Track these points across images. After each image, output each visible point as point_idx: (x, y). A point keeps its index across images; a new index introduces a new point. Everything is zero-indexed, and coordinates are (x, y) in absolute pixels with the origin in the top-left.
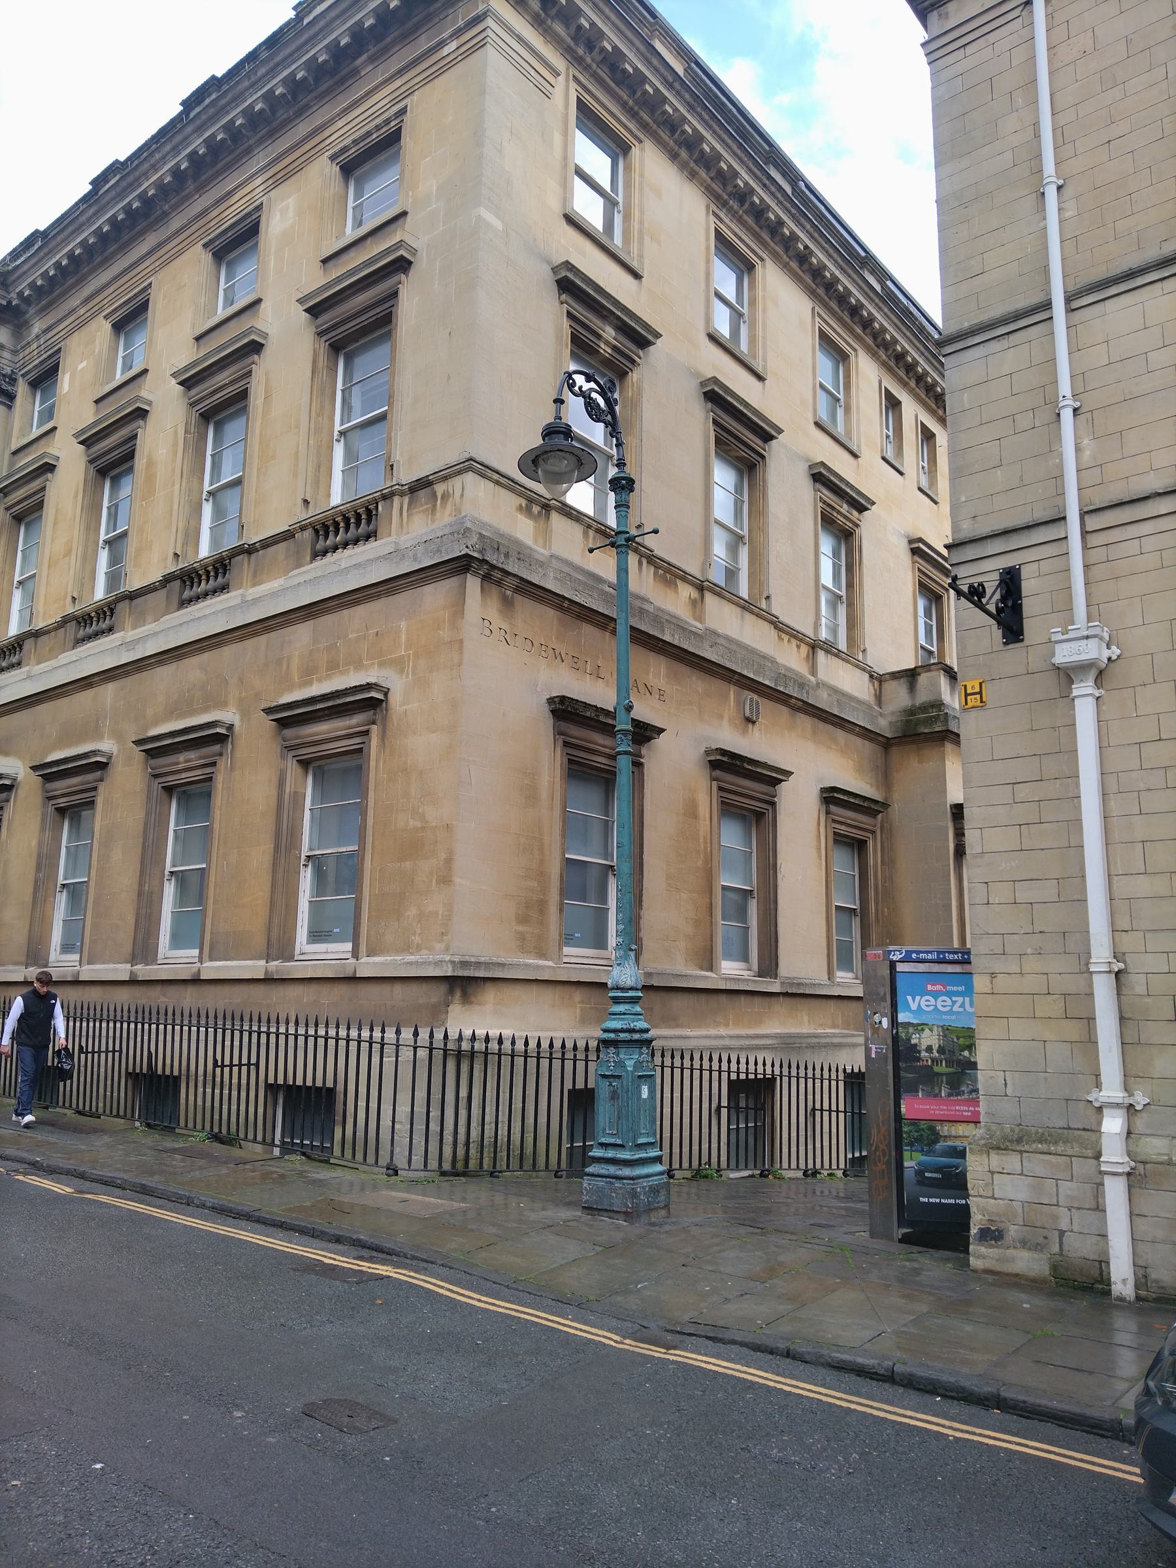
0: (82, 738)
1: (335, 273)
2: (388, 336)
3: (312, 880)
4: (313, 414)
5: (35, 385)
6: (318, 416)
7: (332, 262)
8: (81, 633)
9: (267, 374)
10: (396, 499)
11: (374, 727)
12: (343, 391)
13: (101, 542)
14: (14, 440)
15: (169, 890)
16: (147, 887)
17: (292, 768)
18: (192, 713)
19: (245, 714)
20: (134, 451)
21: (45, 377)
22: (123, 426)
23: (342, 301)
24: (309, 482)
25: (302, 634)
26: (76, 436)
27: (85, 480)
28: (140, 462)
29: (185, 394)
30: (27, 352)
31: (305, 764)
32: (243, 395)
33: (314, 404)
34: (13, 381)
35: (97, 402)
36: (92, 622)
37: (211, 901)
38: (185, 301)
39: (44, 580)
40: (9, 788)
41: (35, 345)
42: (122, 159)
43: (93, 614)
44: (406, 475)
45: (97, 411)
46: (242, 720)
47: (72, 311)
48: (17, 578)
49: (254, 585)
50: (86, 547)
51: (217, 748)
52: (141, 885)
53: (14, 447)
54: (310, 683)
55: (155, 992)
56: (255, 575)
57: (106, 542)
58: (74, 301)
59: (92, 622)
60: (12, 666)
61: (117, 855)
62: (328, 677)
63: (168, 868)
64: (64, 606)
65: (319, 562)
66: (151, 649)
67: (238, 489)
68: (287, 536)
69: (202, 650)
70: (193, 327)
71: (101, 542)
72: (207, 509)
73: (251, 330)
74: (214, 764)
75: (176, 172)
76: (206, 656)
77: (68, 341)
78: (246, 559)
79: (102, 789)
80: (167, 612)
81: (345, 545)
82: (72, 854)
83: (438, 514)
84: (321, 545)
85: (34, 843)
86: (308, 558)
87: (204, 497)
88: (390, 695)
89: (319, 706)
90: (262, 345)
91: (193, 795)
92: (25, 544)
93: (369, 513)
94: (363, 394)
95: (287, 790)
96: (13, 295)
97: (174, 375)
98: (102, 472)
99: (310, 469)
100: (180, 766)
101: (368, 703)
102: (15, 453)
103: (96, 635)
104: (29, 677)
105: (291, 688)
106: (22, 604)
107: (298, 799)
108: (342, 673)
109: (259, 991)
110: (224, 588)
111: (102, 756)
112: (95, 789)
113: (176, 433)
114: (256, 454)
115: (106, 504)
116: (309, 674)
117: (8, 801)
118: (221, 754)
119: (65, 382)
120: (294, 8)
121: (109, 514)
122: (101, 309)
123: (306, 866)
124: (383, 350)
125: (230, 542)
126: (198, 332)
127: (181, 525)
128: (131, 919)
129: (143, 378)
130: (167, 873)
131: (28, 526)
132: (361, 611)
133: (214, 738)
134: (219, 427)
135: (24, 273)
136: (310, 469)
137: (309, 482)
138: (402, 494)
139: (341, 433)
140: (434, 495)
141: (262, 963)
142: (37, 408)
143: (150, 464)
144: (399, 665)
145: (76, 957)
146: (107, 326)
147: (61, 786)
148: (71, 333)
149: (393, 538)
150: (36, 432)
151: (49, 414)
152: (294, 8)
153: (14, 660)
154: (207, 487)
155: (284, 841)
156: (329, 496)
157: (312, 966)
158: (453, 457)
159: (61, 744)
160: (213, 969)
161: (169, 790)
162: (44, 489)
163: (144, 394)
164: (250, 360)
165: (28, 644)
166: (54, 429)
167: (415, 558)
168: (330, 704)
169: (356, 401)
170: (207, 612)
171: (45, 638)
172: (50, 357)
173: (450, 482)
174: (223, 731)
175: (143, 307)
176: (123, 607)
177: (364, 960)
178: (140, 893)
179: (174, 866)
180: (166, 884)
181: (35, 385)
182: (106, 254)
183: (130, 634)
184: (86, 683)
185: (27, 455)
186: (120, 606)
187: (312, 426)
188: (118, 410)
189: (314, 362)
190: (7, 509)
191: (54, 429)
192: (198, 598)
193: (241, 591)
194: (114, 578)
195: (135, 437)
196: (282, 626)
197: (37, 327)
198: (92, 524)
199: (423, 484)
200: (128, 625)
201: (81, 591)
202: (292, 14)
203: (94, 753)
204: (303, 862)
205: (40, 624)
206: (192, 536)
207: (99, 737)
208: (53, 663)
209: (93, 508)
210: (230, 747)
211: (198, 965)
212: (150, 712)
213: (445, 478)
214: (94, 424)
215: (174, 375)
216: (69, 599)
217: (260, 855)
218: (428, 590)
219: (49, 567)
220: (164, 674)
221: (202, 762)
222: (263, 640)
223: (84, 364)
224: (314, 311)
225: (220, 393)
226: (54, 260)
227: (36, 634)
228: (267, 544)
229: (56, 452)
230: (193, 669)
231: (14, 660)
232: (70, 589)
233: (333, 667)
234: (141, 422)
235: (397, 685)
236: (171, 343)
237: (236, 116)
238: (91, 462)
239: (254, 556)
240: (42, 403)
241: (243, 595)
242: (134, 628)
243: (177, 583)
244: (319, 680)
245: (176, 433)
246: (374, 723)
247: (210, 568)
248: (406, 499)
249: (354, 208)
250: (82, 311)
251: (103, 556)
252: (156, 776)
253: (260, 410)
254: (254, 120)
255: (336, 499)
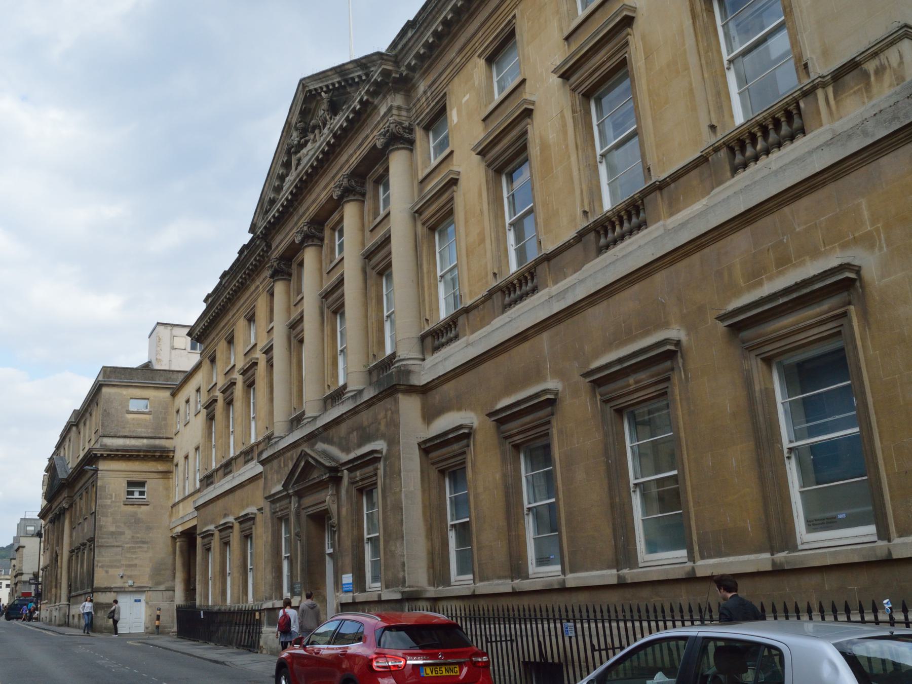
0: (526, 382)
1: (574, 48)
2: (626, 75)
3: (534, 521)
4: (702, 52)
5: (427, 129)
6: (706, 52)
7: (573, 38)
8: (507, 299)
9: (643, 38)
10: (820, 93)
11: (852, 307)
12: (598, 125)
13: (507, 225)
14: (420, 172)
15: (530, 523)
16: (617, 500)
17: (756, 366)
18: (632, 339)
19: (690, 328)
20: (526, 144)
21: (437, 117)
22: (518, 123)
23: (588, 59)
24: (712, 109)
25: (741, 241)
26: (474, 149)
27: (487, 181)
28: (534, 150)
29: (564, 84)
30: (418, 106)
31: (768, 361)
32: (623, 63)
33: (701, 44)
34: (411, 130)
35: (484, 120)
36: (513, 291)
37: (691, 504)
38: (470, 97)
39: (465, 267)
40: (467, 436)
41: (424, 99)
42: (411, 19)
43: (515, 282)
44: (821, 68)
45: (486, 127)
46: (688, 335)
47: (452, 62)
48: (439, 274)
49: (672, 214)
50: (497, 232)
51: (668, 364)
52: (612, 498)
53: (421, 177)
54: (760, 284)
55: (645, 593)
56: (670, 205)
57: (511, 224)
58: (451, 54)
59: (513, 291)
60: (450, 341)
61: (580, 475)
62: (780, 273)
63: (632, 481)
64: (487, 282)
65: (742, 175)
66: (580, 294)
67: (532, 215)
68: (702, 160)
69: (633, 283)
70: (561, 30)
71: (507, 225)
72: (603, 170)
73: (451, 172)
74: (668, 379)
75: (445, 22)
76: (637, 287)
77: (450, 86)
78: (659, 195)
79: (554, 422)
80: (587, 260)
81: (631, 233)
82: (456, 502)
83: (875, 90)
84: (603, 241)
85: (498, 476)
86: (729, 174)
87: (598, 160)
88: (863, 272)
89: (781, 301)
90: (532, 110)
91: (538, 449)
92: (440, 247)
93: (789, 115)
94: (737, 25)
95: (757, 388)
96: (403, 68)
97: (554, 72)
98: (499, 172)
99: (710, 98)
100: (632, 388)
101: (844, 284)
102: (421, 182)
103: (521, 298)
104: (468, 345)
105: (738, 293)
106: (446, 293)
107: (769, 394)
108: (795, 266)
109: (766, 585)
110: (534, 290)
111: (551, 393)
112: (549, 422)
113: (563, 117)
114: (648, 107)
115: (505, 195)
116: (755, 276)
117: (468, 446)
118: (672, 369)
119: (453, 116)
120: (205, 301)
121: (509, 202)
122: (475, 51)
123: (789, 458)
124: (627, 83)
125: (532, 255)
126: (566, 34)
127: (584, 187)
128: (608, 531)
129: (522, 87)
130: (632, 485)
131: (598, 102)
132: (805, 202)
133: (667, 356)
134: (598, 102)
135: (410, 49)
136: (710, 98)
137: (712, 109)
138: (824, 85)
139: (602, 156)
140: (866, 75)
141: (767, 556)
142: (432, 145)
143: (545, 147)
144: (868, 241)
145: (470, 576)
146: (482, 62)
147: (514, 426)
148: (451, 80)
149: (826, 127)
150: (434, 163)
151: (444, 144)
152: (205, 301)
153: (452, 335)
154: (599, 151)
155: (764, 437)
156: (732, 116)
157: (830, 553)
158: (879, 31)
159: (507, 392)
160: (574, 579)
161: (517, 447)
162: (452, 199)
163: (527, 96)
164: (624, 33)
165: (461, 320)
166: (452, 152)
167: (865, 133)
168: (794, 295)
169: (609, 132)
170: (630, 249)
171: (475, 312)
172: (437, 103)
173: (882, 56)
174: (672, 348)
175: (512, 34)
176: (543, 269)
177: (897, 541)
178: (612, 506)
179: (529, 503)
180: (633, 494)
181: (427, 129)
182: (470, 11)
183: (554, 289)
184: (522, 337)
185: (433, 179)
186: (539, 269)
187: (704, 62)
188: (508, 117)
189: (693, 10)
190: (423, 224)
191: (452, 152)
192: (615, 242)
193: (661, 223)
194: (521, 253)
195: (526, 132)
196: (716, 240)
197: (422, 87)
198: (498, 214)
199: (853, 66)
200: (550, 282)
201: (500, 267)
202: (204, 306)
203: (545, 391)
204: (786, 455)
205: (468, 302)
206: (595, 193)
207: (544, 379)
208: (487, 329)
209: (496, 200)
210: (680, 361)
211: (562, 577)
212: (587, 348)
213: (875, 54)
214: (489, 135)
215: (554, 72)
216: (490, 276)
217: (738, 456)
218: (885, 161)
219: (468, 256)
220: (596, 312)
221: (654, 380)
222: (695, 258)
223: (467, 97)
224: (565, 76)
225: (507, 153)
226: (431, 30)
227: (467, 311)
228: (676, 177)
229: (456, 168)
230: (627, 303)
231: (452, 335)
232: (489, 266)
233: (784, 262)
234: (529, 120)
235: (869, 262)
236: (466, 124)
237: (428, 37)
238: (488, 166)
239: (665, 191)
240: (434, 140)
241: (664, 225)
242: (556, 282)
243: (592, 236)
244: (770, 279)
245: (563, 117)
246: (850, 303)
247: (623, 213)
248: (830, 90)
249: (498, 82)
250: (458, 60)
251: (511, 237)
252: (506, 438)
253: (643, 70)
254: (429, 47)
255: (739, 118)
